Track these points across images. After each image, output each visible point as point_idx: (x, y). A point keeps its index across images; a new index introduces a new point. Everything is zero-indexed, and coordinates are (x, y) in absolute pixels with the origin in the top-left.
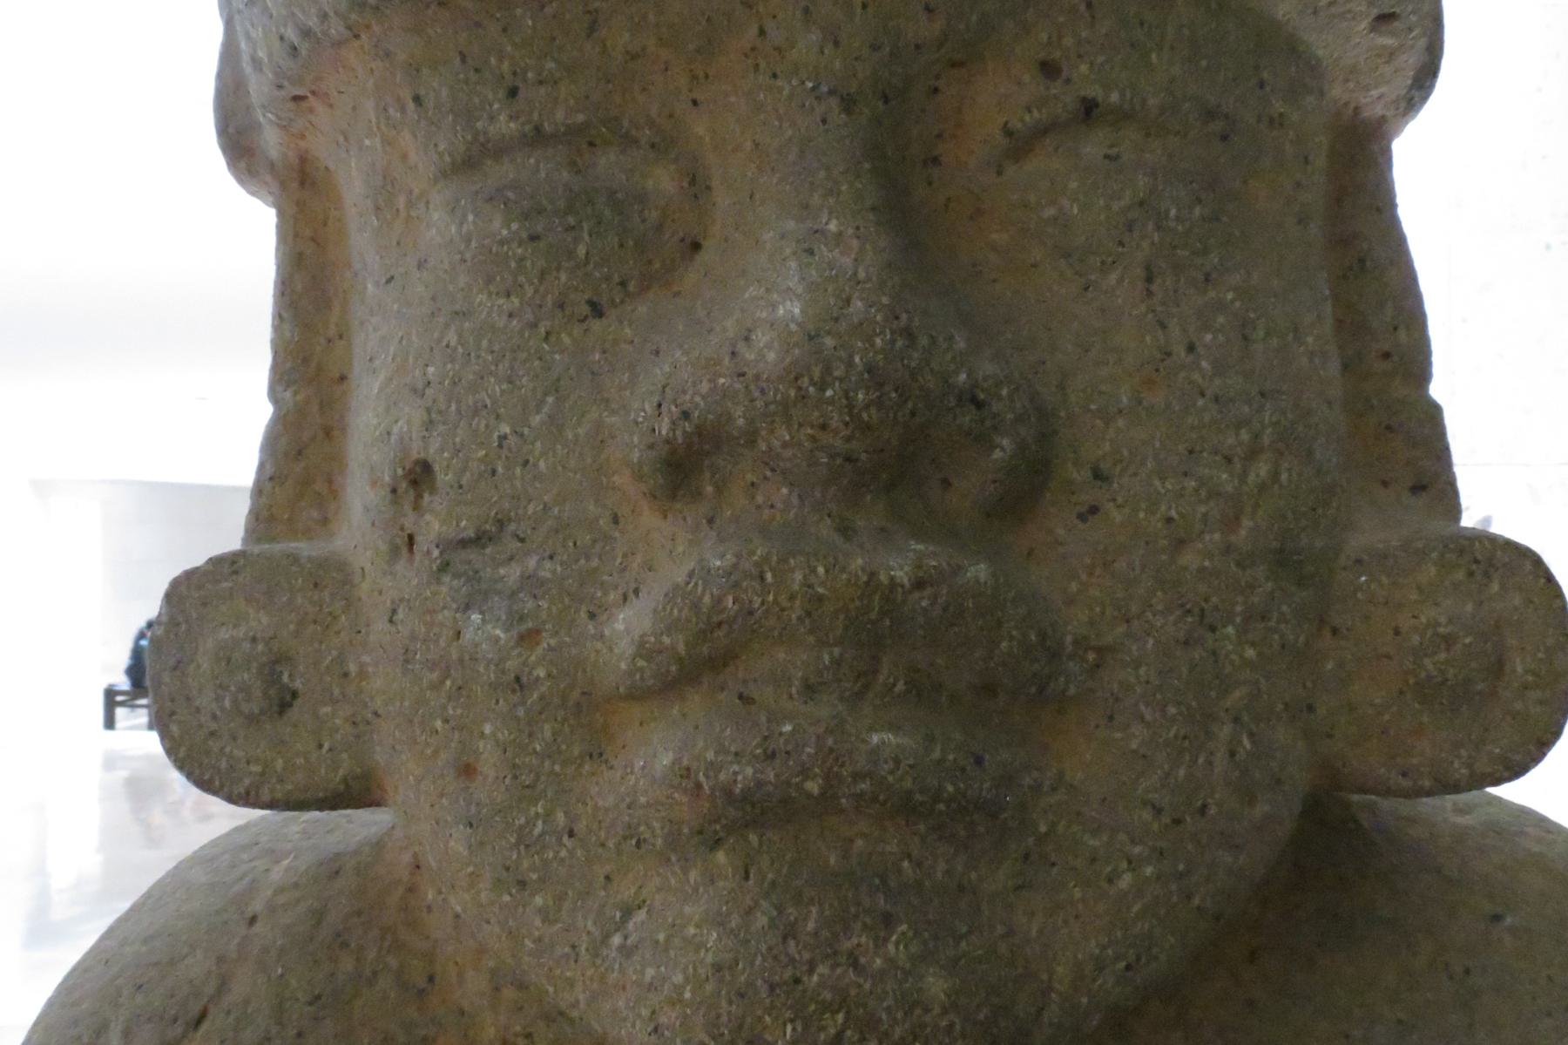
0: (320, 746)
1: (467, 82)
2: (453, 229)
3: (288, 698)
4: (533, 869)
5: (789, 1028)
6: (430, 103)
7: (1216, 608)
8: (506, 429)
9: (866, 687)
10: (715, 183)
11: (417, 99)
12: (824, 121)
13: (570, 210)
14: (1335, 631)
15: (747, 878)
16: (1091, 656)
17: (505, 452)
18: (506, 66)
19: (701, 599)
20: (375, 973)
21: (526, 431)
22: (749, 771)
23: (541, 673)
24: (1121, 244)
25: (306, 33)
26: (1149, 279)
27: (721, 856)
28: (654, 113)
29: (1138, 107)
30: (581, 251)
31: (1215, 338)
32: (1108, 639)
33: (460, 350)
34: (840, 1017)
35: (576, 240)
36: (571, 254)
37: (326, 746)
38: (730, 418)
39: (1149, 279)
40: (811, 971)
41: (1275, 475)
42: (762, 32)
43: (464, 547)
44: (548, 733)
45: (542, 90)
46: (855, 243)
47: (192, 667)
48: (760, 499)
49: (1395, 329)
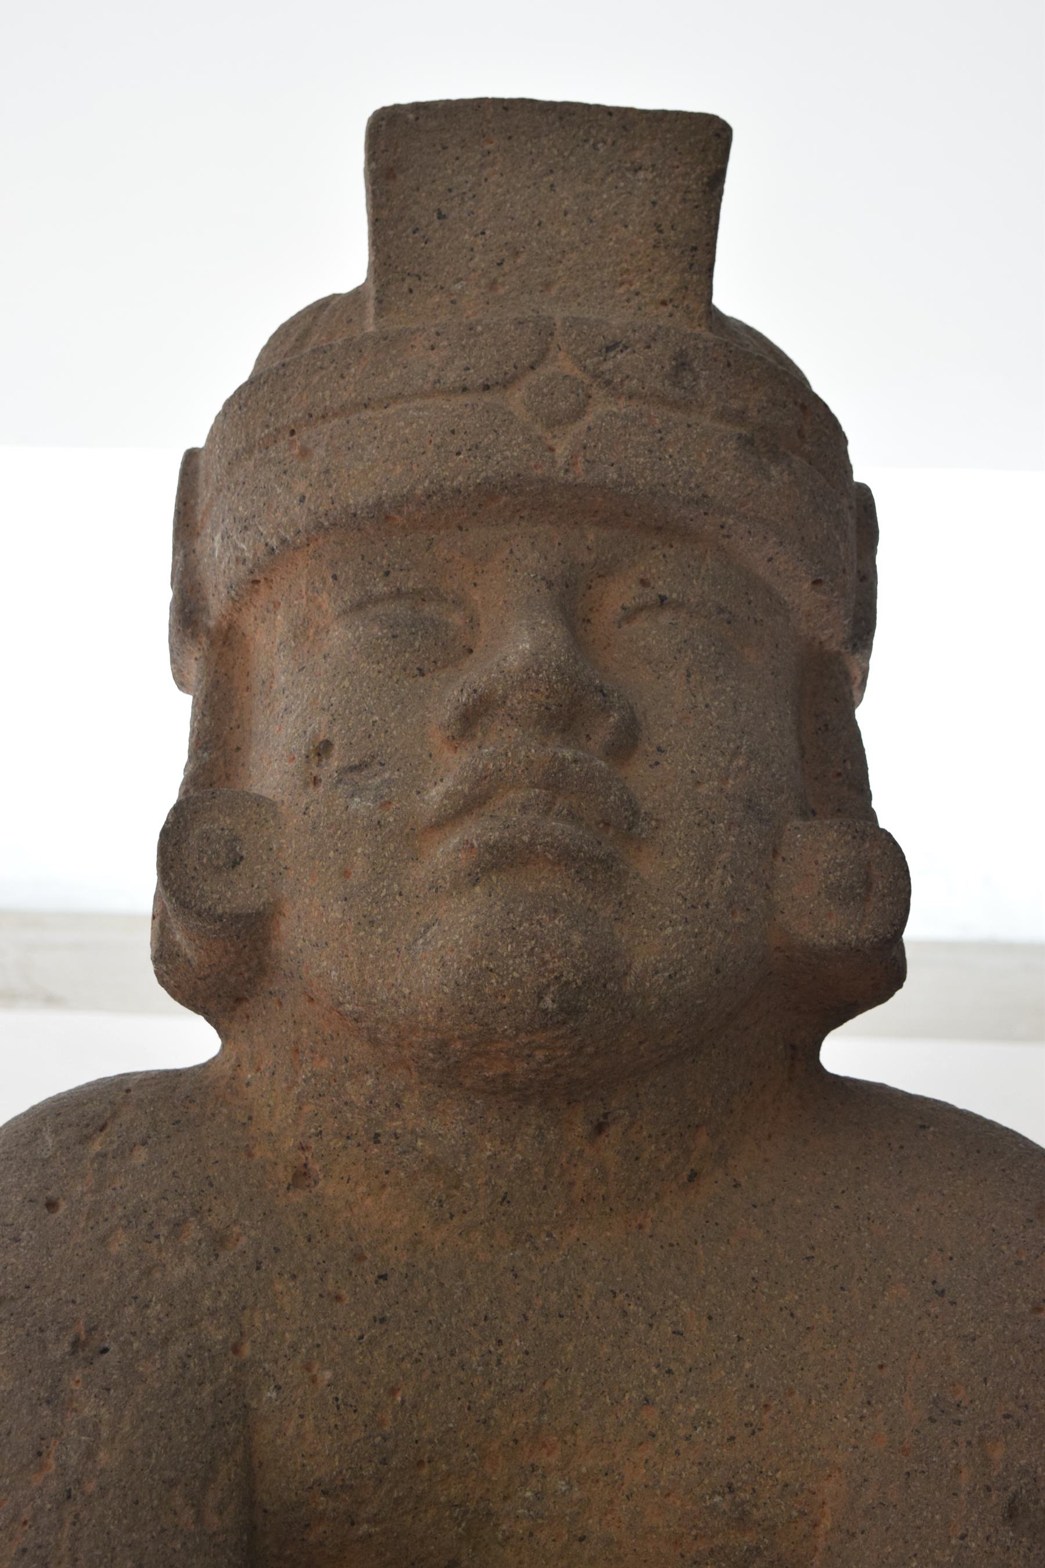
0: (253, 886)
1: (364, 568)
2: (350, 635)
3: (238, 860)
4: (379, 913)
5: (510, 946)
6: (342, 579)
7: (714, 813)
8: (377, 718)
9: (550, 809)
10: (482, 622)
11: (335, 577)
12: (538, 591)
13: (413, 625)
14: (784, 859)
15: (490, 896)
16: (653, 823)
17: (375, 728)
18: (385, 562)
19: (477, 766)
20: (213, 1115)
21: (387, 719)
22: (497, 834)
23: (391, 819)
24: (675, 658)
25: (283, 541)
26: (689, 676)
27: (478, 889)
28: (455, 587)
29: (686, 602)
30: (417, 644)
31: (719, 704)
32: (661, 816)
33: (351, 688)
34: (533, 942)
35: (415, 639)
36: (412, 645)
37: (256, 886)
38: (496, 691)
39: (689, 676)
40: (520, 925)
41: (748, 767)
42: (511, 552)
43: (351, 771)
44: (392, 848)
45: (402, 573)
46: (553, 628)
47: (185, 845)
48: (504, 735)
49: (845, 761)
